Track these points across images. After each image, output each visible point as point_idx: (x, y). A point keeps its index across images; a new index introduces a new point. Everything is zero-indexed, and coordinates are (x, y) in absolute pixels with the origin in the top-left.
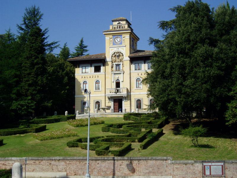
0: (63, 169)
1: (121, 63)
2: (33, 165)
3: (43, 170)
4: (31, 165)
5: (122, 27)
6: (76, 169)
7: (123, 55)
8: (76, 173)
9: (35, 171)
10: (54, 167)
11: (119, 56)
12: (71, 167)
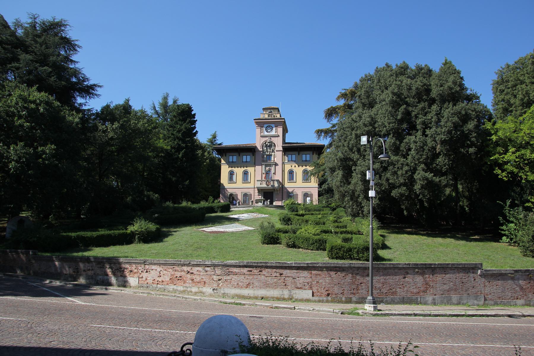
0: (306, 284)
1: (273, 154)
2: (247, 277)
3: (266, 286)
4: (243, 277)
5: (274, 116)
6: (329, 284)
7: (275, 146)
8: (329, 292)
9: (251, 287)
10: (289, 281)
11: (270, 146)
12: (320, 281)
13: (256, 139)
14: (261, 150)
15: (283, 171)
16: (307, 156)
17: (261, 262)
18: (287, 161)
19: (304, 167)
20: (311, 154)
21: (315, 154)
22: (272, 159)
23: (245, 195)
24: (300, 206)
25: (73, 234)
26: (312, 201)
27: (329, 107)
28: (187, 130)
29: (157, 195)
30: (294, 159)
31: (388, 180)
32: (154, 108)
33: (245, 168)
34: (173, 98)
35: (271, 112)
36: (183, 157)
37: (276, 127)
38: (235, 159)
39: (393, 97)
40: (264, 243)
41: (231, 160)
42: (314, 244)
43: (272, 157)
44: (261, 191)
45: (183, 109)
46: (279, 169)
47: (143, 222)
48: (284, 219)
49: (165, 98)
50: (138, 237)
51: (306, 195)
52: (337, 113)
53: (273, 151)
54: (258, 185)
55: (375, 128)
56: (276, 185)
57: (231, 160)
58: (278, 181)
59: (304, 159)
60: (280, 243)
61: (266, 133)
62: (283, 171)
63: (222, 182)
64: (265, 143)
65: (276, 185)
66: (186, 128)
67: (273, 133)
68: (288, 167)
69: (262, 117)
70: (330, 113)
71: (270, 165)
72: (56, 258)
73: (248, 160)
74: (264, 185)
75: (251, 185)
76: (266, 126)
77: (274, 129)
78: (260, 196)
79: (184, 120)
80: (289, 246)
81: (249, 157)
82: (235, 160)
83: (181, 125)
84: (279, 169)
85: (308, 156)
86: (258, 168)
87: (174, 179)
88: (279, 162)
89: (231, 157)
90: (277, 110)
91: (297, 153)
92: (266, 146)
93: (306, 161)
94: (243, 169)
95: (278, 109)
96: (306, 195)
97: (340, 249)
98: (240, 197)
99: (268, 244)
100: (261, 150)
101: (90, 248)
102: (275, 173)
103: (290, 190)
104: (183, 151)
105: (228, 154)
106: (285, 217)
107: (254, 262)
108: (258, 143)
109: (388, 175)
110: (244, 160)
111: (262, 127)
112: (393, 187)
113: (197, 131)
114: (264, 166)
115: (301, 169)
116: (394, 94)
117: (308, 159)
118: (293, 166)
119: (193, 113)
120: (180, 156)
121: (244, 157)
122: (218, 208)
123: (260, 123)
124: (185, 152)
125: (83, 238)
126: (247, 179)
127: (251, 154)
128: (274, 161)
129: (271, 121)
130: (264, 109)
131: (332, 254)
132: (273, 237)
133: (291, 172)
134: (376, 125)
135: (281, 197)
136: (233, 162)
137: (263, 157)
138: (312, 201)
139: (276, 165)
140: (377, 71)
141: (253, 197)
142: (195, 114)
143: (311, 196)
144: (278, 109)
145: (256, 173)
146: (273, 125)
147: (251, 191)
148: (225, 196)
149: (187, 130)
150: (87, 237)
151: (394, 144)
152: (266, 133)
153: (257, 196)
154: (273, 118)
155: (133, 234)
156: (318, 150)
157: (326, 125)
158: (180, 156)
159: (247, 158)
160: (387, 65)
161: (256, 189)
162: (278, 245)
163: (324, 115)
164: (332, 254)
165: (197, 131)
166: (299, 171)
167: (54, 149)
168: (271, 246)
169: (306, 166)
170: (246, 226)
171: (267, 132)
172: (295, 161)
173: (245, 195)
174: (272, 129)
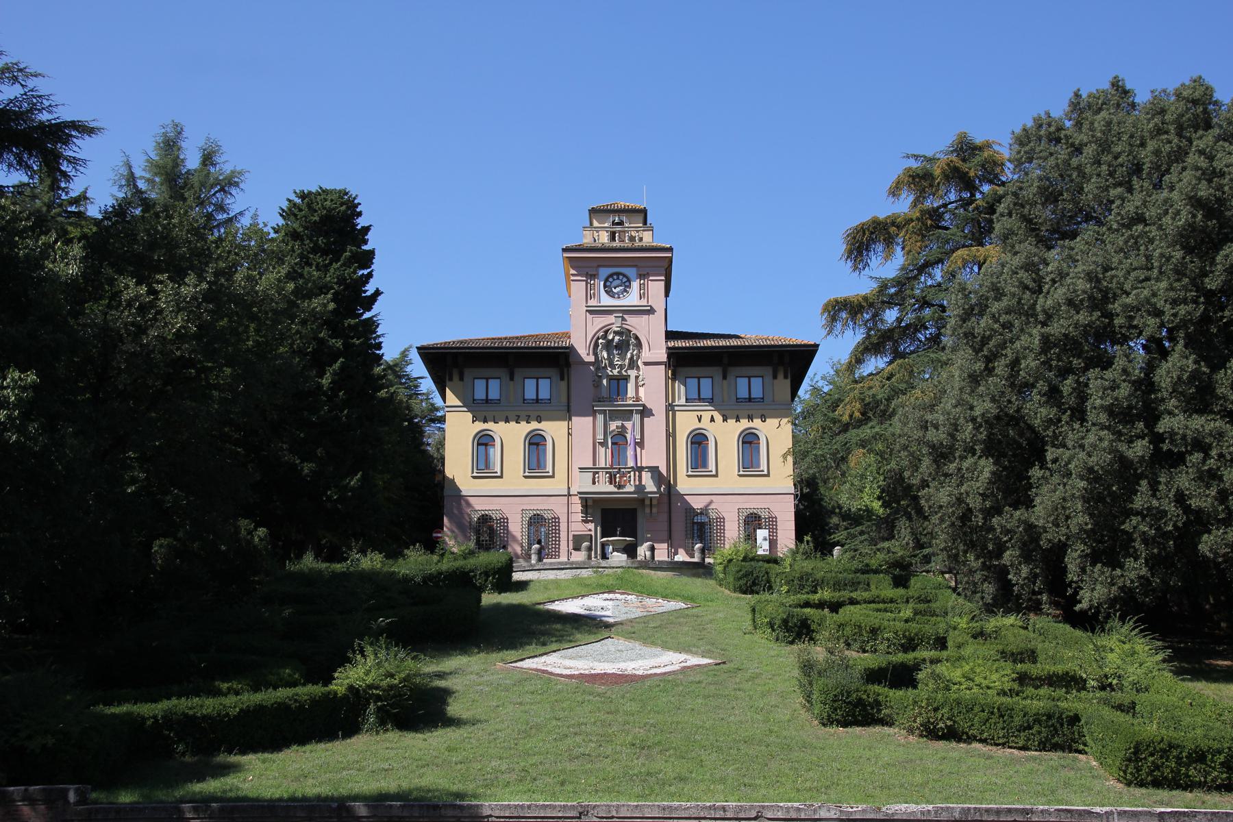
1: (633, 373)
5: (632, 239)
7: (639, 345)
11: (622, 347)
13: (573, 318)
14: (591, 359)
15: (671, 435)
16: (751, 384)
17: (1009, 811)
18: (683, 401)
19: (745, 424)
20: (769, 378)
21: (781, 376)
22: (631, 392)
23: (536, 521)
24: (775, 569)
25: (146, 709)
26: (773, 543)
28: (347, 287)
29: (262, 531)
30: (707, 393)
31: (1180, 498)
32: (131, 179)
33: (534, 425)
34: (201, 143)
35: (621, 223)
36: (336, 385)
37: (642, 276)
39: (1194, 216)
40: (828, 722)
41: (480, 394)
42: (1030, 728)
43: (631, 387)
44: (595, 507)
45: (330, 210)
46: (655, 427)
47: (382, 654)
48: (785, 622)
49: (170, 145)
50: (379, 709)
51: (752, 521)
52: (889, 241)
53: (633, 364)
54: (583, 484)
55: (1110, 316)
56: (650, 485)
57: (480, 394)
58: (654, 470)
59: (743, 392)
60: (886, 722)
61: (606, 300)
62: (671, 435)
63: (449, 473)
64: (605, 337)
65: (650, 485)
67: (632, 298)
68: (686, 423)
69: (587, 240)
70: (864, 241)
71: (627, 415)
72: (195, 809)
73: (544, 394)
75: (557, 485)
76: (604, 272)
77: (635, 285)
78: (591, 526)
79: (334, 253)
80: (931, 733)
81: (545, 384)
82: (494, 394)
83: (326, 268)
84: (655, 427)
85: (757, 384)
86: (582, 424)
87: (307, 468)
88: (657, 405)
89: (480, 385)
91: (717, 371)
92: (609, 345)
93: (750, 400)
94: (524, 428)
95: (644, 212)
96: (752, 521)
97: (1165, 753)
98: (517, 527)
99: (845, 725)
100: (591, 359)
101: (222, 758)
102: (640, 444)
103: (697, 504)
104: (337, 366)
105: (468, 373)
106: (790, 616)
107: (988, 811)
109: (1184, 480)
110: (530, 394)
111: (593, 277)
112: (1199, 522)
113: (378, 293)
114: (600, 418)
115: (735, 428)
116: (1196, 202)
117: (757, 392)
118: (706, 416)
119: (361, 222)
120: (326, 381)
121: (530, 385)
122: (486, 574)
123: (585, 264)
124: (342, 368)
125: (188, 725)
127: (553, 372)
128: (638, 399)
130: (594, 212)
131: (1138, 770)
132: (860, 702)
133: (698, 441)
134: (1116, 307)
135: (665, 527)
136: (487, 401)
137: (598, 385)
138: (773, 543)
139: (645, 412)
140: (1078, 106)
142: (366, 229)
143: (772, 524)
144: (644, 212)
145: (575, 441)
146: (631, 272)
147: (557, 508)
148: (462, 526)
149: (347, 287)
150: (204, 717)
151: (1195, 375)
152: (606, 300)
153: (576, 523)
154: (627, 244)
155: (357, 699)
156: (793, 361)
157: (860, 285)
158: (326, 381)
159: (538, 387)
160: (1116, 84)
161: (576, 500)
162: (877, 729)
163: (842, 248)
164: (1138, 770)
166: (725, 434)
167: (34, 386)
168: (1054, 757)
169: (750, 418)
170: (666, 647)
171: (610, 293)
172: (711, 401)
173: (536, 521)
174: (627, 285)
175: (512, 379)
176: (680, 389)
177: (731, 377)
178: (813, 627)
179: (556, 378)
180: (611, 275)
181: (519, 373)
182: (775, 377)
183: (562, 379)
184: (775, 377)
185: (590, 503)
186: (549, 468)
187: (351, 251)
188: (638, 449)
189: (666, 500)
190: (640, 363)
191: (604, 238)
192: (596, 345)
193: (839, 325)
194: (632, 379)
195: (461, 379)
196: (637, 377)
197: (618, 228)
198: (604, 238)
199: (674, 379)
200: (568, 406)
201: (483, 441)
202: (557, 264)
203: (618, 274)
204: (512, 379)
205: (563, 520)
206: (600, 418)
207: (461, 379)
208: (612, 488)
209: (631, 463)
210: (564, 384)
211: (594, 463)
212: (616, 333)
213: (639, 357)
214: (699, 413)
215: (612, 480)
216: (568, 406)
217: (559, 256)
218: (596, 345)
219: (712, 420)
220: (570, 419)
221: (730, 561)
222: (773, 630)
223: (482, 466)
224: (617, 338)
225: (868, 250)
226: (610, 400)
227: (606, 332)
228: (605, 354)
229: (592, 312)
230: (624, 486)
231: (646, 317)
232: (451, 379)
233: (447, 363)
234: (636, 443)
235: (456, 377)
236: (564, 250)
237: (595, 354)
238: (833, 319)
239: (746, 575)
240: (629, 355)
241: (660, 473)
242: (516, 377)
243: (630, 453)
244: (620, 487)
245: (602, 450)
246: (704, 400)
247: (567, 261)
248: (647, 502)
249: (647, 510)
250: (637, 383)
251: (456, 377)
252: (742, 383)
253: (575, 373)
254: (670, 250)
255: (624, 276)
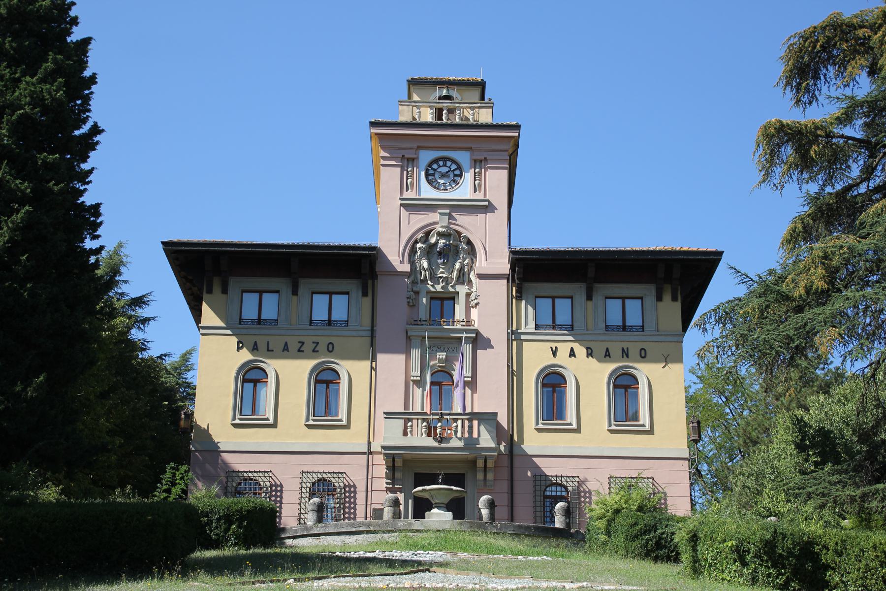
1: (462, 290)
11: (449, 254)
14: (406, 268)
15: (514, 373)
18: (531, 327)
20: (650, 300)
21: (667, 297)
27: (818, 18)
30: (564, 317)
35: (448, 98)
38: (271, 307)
41: (250, 311)
44: (407, 469)
46: (492, 364)
53: (463, 278)
54: (390, 434)
56: (486, 441)
57: (250, 311)
58: (488, 418)
61: (428, 192)
62: (514, 373)
65: (486, 441)
66: (37, 100)
67: (464, 190)
68: (536, 357)
69: (405, 116)
74: (419, 439)
75: (353, 439)
82: (270, 310)
85: (634, 307)
86: (392, 364)
88: (495, 328)
89: (250, 303)
90: (475, 94)
91: (578, 290)
92: (430, 251)
93: (624, 328)
94: (307, 365)
95: (481, 85)
100: (406, 268)
102: (472, 384)
104: (18, 217)
105: (235, 284)
108: (391, 236)
110: (320, 312)
114: (416, 354)
118: (564, 349)
119: (77, 35)
122: (228, 519)
123: (400, 144)
124: (27, 226)
126: (329, 409)
127: (352, 285)
128: (469, 322)
129: (449, 136)
130: (414, 83)
133: (553, 383)
137: (413, 304)
139: (479, 341)
141: (361, 497)
144: (481, 85)
145: (381, 391)
146: (463, 158)
147: (353, 471)
152: (428, 192)
153: (376, 490)
156: (683, 275)
159: (332, 304)
161: (380, 459)
163: (780, 69)
165: (96, 130)
172: (571, 328)
174: (456, 175)
175: (295, 293)
176: (528, 314)
177: (598, 298)
178: (827, 557)
179: (356, 292)
180: (436, 161)
181: (305, 285)
182: (659, 298)
183: (365, 294)
184: (659, 298)
185: (399, 463)
186: (343, 415)
187: (55, 61)
188: (468, 392)
189: (506, 462)
190: (472, 276)
191: (427, 116)
192: (413, 251)
193: (778, 170)
194: (462, 299)
195: (225, 291)
196: (468, 295)
197: (446, 104)
198: (427, 116)
199: (519, 298)
200: (372, 330)
201: (252, 375)
202: (363, 139)
203: (445, 159)
204: (295, 293)
205: (361, 487)
206: (416, 354)
207: (225, 291)
208: (430, 442)
209: (457, 408)
210: (367, 301)
211: (406, 406)
212: (440, 235)
213: (471, 268)
214: (554, 345)
215: (430, 431)
216: (372, 330)
217: (366, 132)
218: (413, 251)
219: (572, 354)
220: (374, 359)
221: (617, 511)
222: (744, 564)
223: (247, 410)
224: (442, 242)
225: (816, 77)
226: (433, 322)
227: (428, 234)
228: (425, 264)
229: (410, 207)
230: (448, 439)
231: (481, 216)
232: (210, 291)
233: (202, 269)
234: (466, 384)
235: (217, 289)
236: (374, 124)
237: (412, 263)
238: (773, 156)
239: (646, 531)
240: (458, 265)
241: (498, 426)
242: (301, 291)
243: (457, 394)
244: (441, 440)
245: (418, 392)
246: (561, 327)
247: (376, 141)
248: (480, 464)
249: (480, 476)
250: (468, 302)
251: (217, 289)
252: (614, 306)
253: (382, 285)
254: (517, 127)
255: (454, 161)
